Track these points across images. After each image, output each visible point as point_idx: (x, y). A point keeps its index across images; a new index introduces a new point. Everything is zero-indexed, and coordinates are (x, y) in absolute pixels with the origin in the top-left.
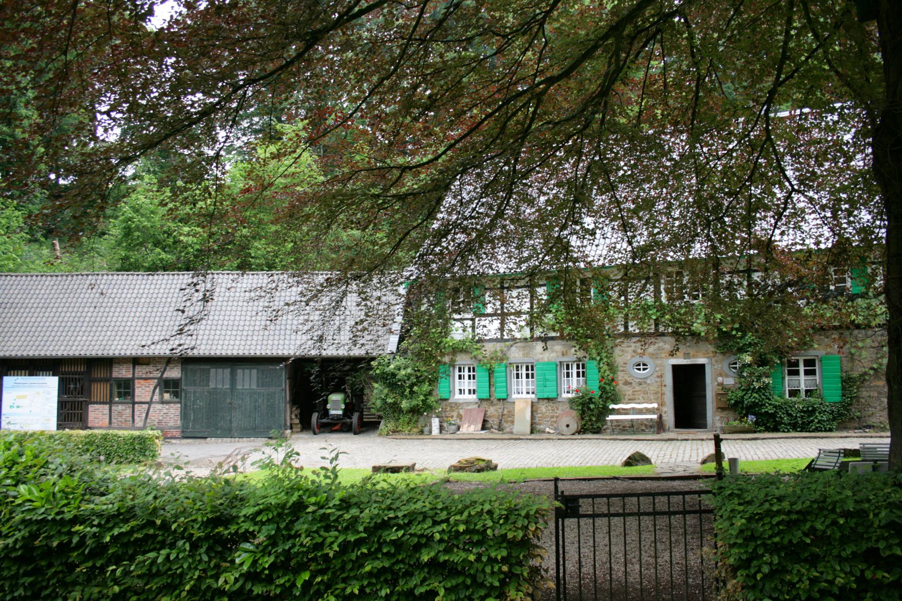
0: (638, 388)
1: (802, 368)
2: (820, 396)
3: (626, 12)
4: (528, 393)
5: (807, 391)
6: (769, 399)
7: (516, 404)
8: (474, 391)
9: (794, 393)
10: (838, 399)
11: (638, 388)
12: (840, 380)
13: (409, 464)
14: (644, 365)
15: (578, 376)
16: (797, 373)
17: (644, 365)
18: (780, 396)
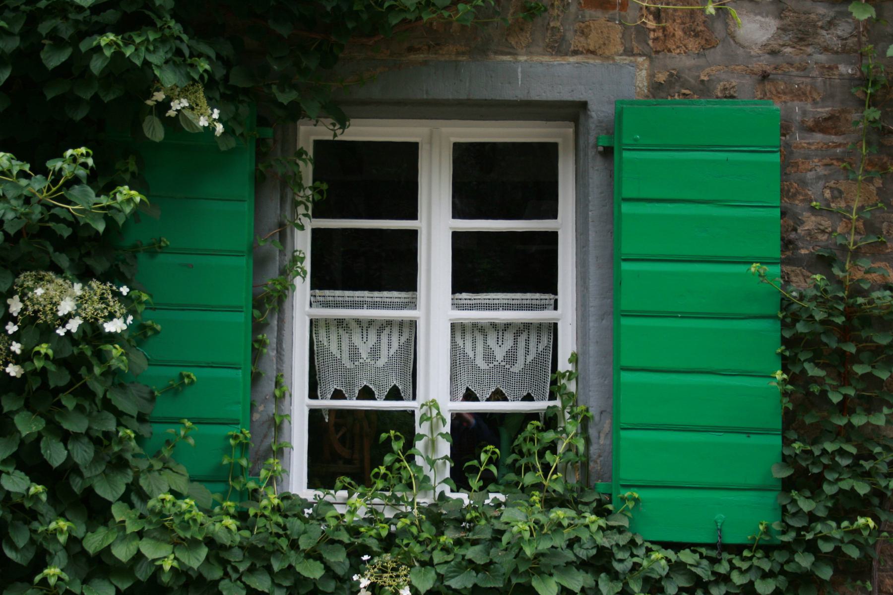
1: (437, 227)
2: (589, 489)
3: (778, 543)
5: (469, 434)
6: (96, 511)
9: (353, 446)
10: (748, 515)
12: (769, 334)
16: (393, 265)
18: (221, 477)
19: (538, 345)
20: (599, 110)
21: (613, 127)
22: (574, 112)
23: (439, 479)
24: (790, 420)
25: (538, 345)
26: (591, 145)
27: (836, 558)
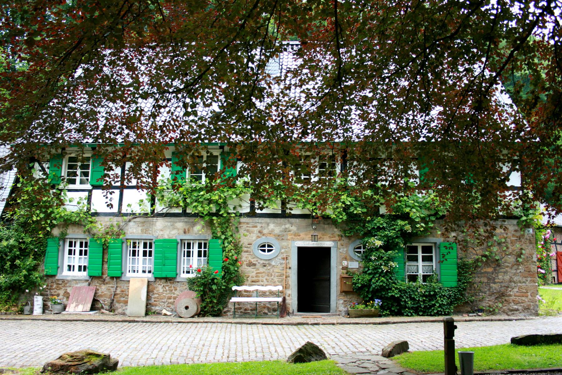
0: (262, 270)
1: (420, 255)
4: (144, 272)
5: (425, 278)
8: (150, 272)
9: (413, 278)
10: (454, 284)
12: (456, 266)
14: (269, 246)
16: (416, 259)
17: (269, 246)
19: (431, 267)
20: (438, 243)
21: (440, 245)
22: (435, 243)
23: (421, 282)
24: (458, 275)
25: (431, 267)
26: (219, 158)
27: (463, 288)
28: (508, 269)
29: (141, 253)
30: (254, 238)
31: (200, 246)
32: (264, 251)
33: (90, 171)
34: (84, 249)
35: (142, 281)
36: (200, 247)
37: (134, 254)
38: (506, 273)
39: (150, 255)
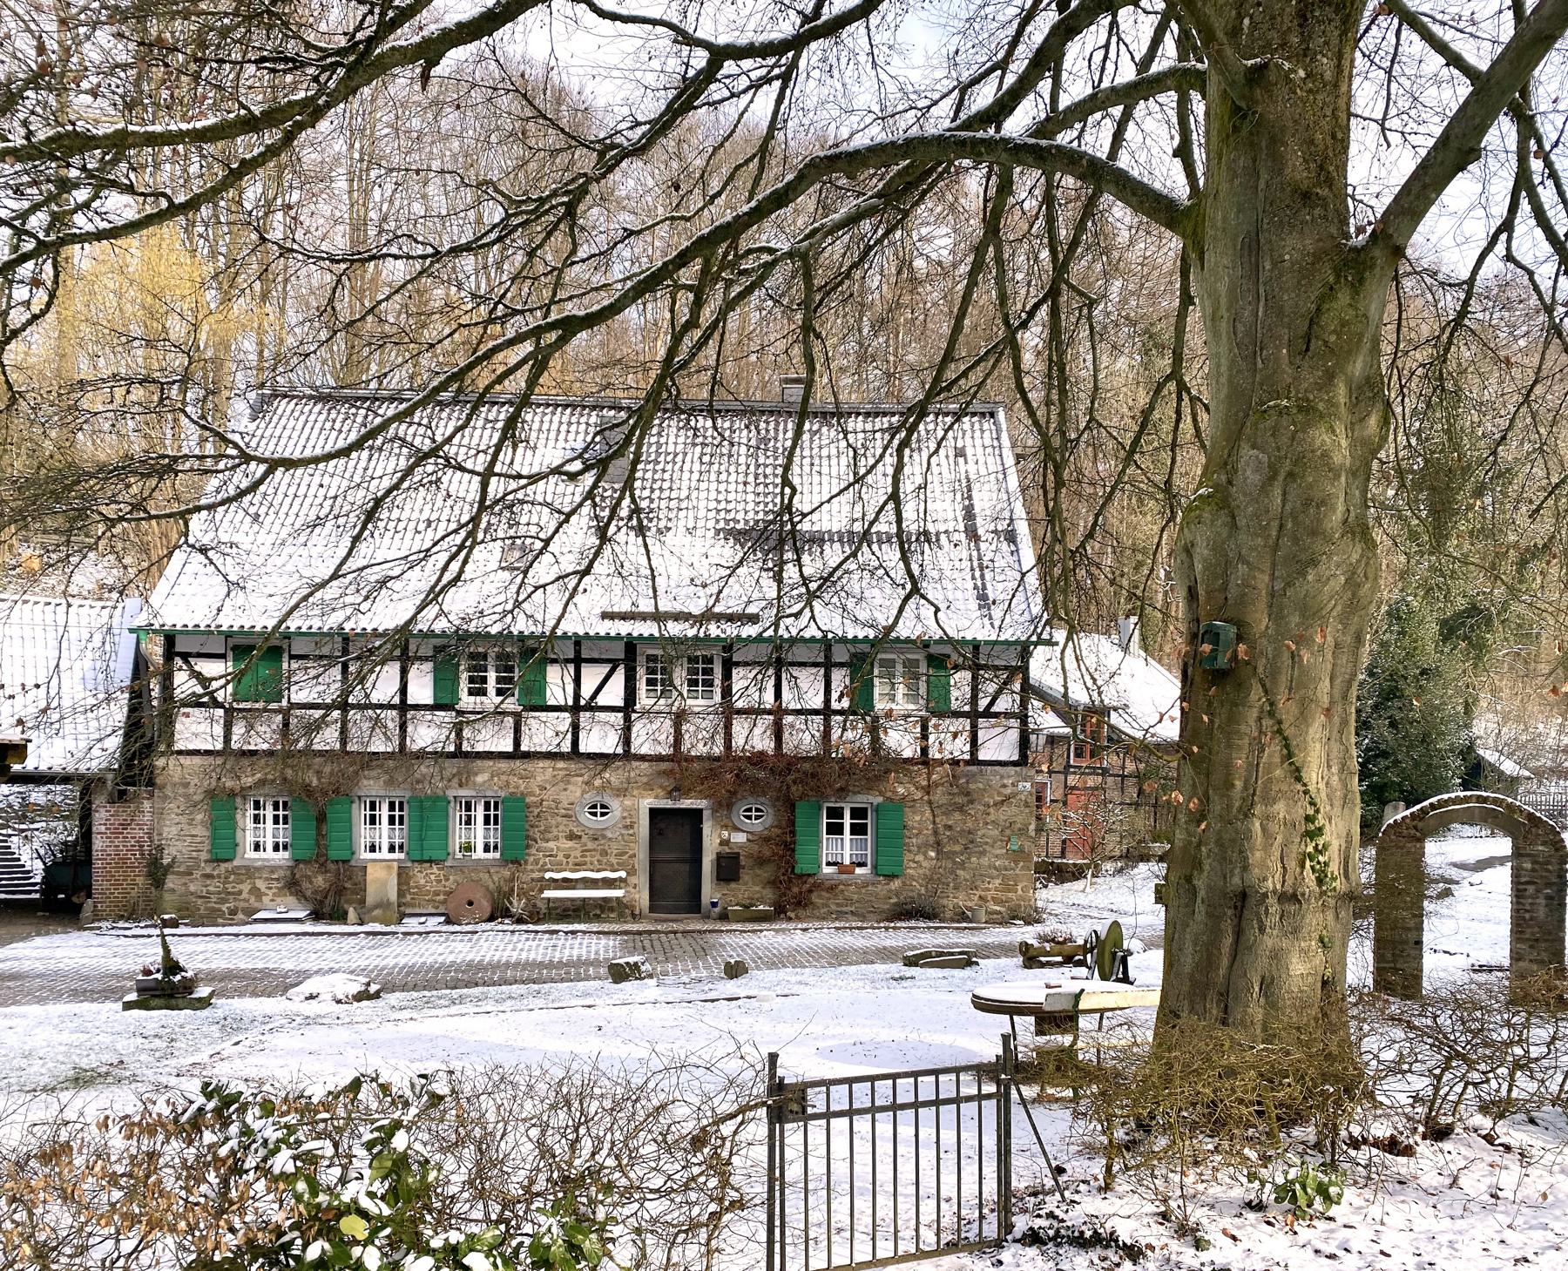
0: (590, 845)
4: (276, 848)
7: (369, 870)
8: (285, 848)
11: (590, 845)
13: (1519, 1266)
14: (603, 807)
15: (276, 821)
17: (603, 807)
28: (988, 848)
29: (385, 820)
30: (578, 794)
31: (487, 807)
32: (595, 814)
33: (869, 821)
34: (281, 813)
35: (389, 867)
36: (487, 807)
37: (373, 821)
38: (983, 853)
39: (401, 823)
